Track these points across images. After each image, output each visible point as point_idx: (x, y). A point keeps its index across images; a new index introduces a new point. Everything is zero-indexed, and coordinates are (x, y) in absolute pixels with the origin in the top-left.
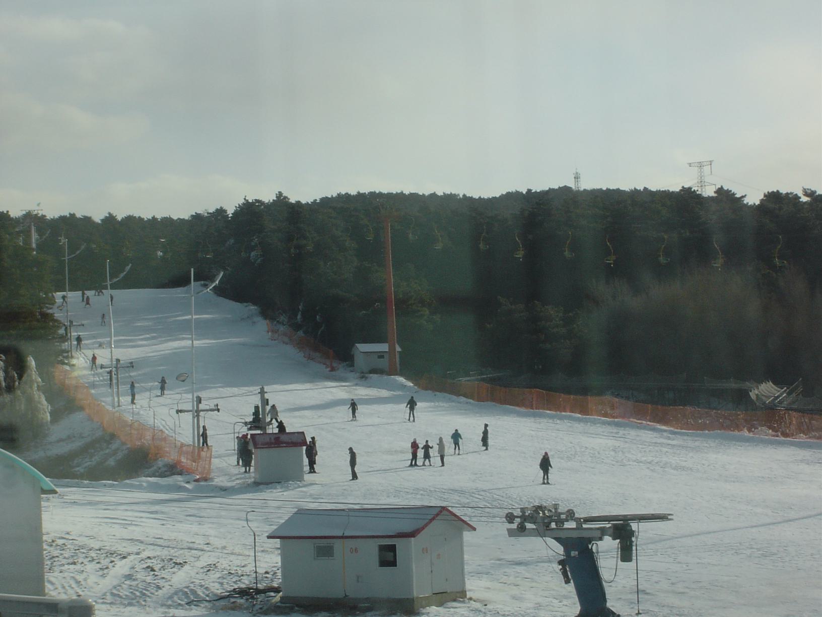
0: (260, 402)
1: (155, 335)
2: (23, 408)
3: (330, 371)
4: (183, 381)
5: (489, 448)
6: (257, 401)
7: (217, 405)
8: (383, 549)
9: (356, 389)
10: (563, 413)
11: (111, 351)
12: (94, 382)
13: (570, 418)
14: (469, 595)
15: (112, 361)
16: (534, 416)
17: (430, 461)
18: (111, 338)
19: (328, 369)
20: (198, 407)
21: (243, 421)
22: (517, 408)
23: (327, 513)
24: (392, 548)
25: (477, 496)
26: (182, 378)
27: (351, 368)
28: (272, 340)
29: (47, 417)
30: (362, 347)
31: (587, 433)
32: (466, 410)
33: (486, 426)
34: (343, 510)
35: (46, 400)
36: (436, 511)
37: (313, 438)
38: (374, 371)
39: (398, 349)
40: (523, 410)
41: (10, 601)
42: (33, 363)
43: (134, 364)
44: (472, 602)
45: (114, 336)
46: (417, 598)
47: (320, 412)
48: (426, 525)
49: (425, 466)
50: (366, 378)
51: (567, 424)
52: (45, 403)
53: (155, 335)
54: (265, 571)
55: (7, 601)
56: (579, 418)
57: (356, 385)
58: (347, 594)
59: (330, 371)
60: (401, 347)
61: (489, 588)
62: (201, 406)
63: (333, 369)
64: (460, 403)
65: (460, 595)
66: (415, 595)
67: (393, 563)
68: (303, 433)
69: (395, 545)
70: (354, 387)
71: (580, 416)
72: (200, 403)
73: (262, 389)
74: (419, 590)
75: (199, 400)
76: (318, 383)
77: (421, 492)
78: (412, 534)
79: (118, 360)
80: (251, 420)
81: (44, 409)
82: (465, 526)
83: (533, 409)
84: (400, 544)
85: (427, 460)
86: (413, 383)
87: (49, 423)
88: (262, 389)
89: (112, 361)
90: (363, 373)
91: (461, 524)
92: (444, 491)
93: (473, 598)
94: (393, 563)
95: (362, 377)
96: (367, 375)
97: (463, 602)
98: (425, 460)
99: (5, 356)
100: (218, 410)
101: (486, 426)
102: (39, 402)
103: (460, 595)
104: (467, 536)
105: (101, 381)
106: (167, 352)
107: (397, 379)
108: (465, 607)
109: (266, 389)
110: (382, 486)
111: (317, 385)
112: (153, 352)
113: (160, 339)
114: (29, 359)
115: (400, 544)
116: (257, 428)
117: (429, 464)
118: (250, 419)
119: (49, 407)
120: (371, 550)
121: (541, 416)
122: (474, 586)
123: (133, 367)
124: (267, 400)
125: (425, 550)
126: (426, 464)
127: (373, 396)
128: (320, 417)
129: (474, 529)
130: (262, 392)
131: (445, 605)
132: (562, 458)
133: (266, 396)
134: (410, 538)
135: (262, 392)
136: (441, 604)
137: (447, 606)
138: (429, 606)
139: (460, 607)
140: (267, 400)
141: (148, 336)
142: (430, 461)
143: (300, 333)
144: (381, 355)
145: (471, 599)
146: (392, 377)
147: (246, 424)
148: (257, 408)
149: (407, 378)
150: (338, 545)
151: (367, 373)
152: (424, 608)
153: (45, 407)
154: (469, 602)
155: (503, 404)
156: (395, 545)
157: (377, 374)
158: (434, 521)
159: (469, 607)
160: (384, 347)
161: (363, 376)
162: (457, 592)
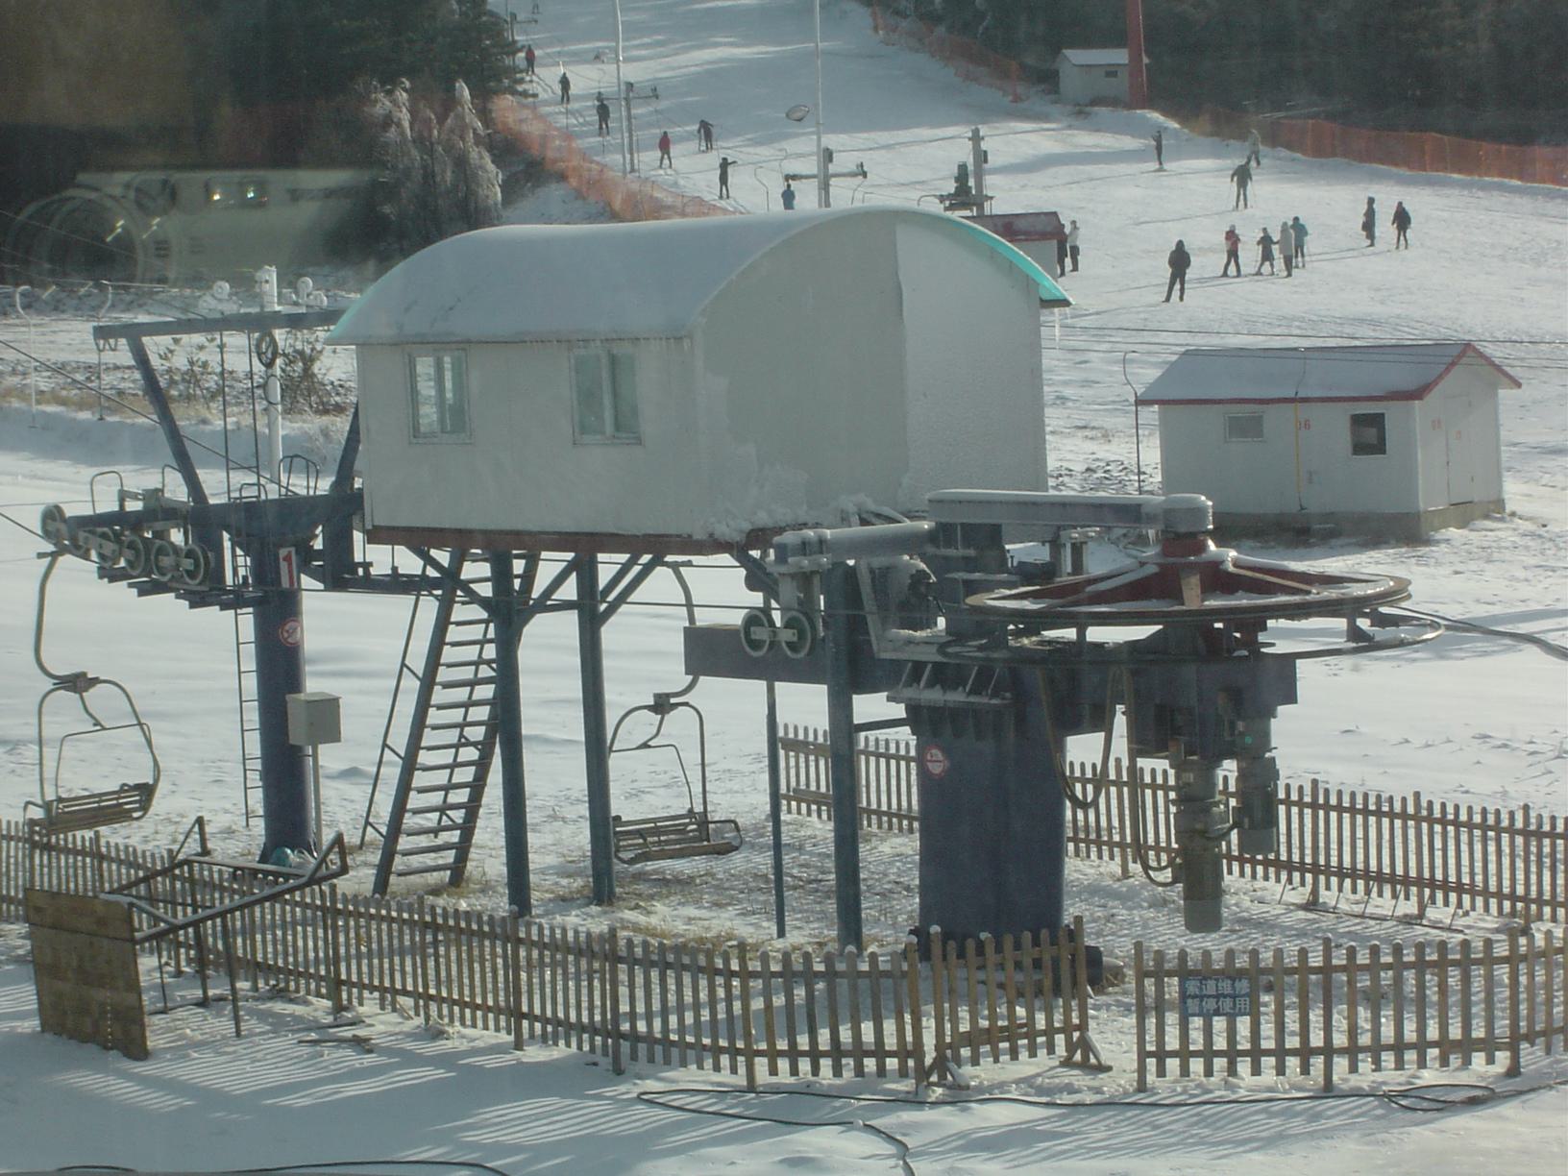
0: (971, 157)
1: (660, 37)
2: (448, 179)
3: (1012, 102)
4: (799, 120)
5: (1376, 241)
6: (964, 153)
7: (862, 165)
8: (1358, 421)
9: (1073, 135)
10: (1487, 179)
11: (618, 67)
12: (567, 127)
13: (1501, 188)
14: (1509, 508)
15: (619, 86)
16: (1430, 183)
17: (1272, 265)
18: (618, 43)
19: (1011, 98)
20: (826, 168)
21: (938, 193)
22: (1394, 170)
23: (1279, 353)
24: (1377, 421)
25: (1406, 329)
26: (799, 115)
27: (1053, 97)
28: (887, 44)
29: (496, 194)
30: (1076, 56)
31: (1545, 215)
32: (1295, 173)
33: (1371, 201)
34: (1295, 349)
35: (493, 162)
36: (1455, 352)
37: (1074, 223)
38: (1096, 102)
39: (1146, 60)
40: (1404, 172)
41: (1034, 504)
42: (466, 93)
43: (659, 92)
44: (1516, 520)
45: (623, 40)
46: (1426, 512)
47: (1022, 179)
48: (1440, 377)
49: (1261, 274)
50: (1088, 114)
51: (1498, 199)
52: (491, 167)
53: (660, 37)
54: (1086, 466)
55: (995, 502)
56: (1518, 187)
57: (1070, 127)
58: (1304, 505)
59: (1012, 102)
60: (1149, 57)
61: (1529, 495)
62: (832, 168)
63: (1017, 99)
64: (1279, 159)
65: (1494, 509)
66: (1422, 506)
67: (1379, 447)
68: (1055, 214)
69: (1383, 415)
70: (1069, 132)
71: (1519, 183)
72: (831, 160)
73: (976, 132)
74: (1429, 499)
75: (828, 156)
76: (997, 125)
77: (1297, 323)
78: (1417, 394)
79: (630, 86)
80: (952, 191)
81: (489, 179)
82: (1505, 380)
83: (1425, 170)
84: (1392, 412)
85: (1267, 263)
86: (1179, 123)
87: (500, 206)
88: (976, 132)
89: (619, 86)
90: (1079, 105)
91: (1499, 375)
92: (1338, 321)
93: (1519, 513)
94: (1379, 447)
95: (1080, 113)
96: (1088, 109)
97: (1502, 520)
98: (1262, 265)
99: (411, 83)
100: (865, 175)
101: (1371, 201)
102: (482, 167)
103: (1494, 509)
104: (1505, 394)
105: (582, 125)
106: (693, 69)
107: (1149, 116)
108: (1507, 528)
109: (983, 130)
110: (1213, 313)
111: (997, 128)
112: (664, 70)
113: (673, 46)
114: (457, 85)
115: (1392, 412)
116: (965, 205)
117: (1235, 274)
118: (951, 187)
119: (500, 176)
120: (1334, 428)
121: (1443, 184)
122: (1514, 491)
123: (657, 97)
124: (985, 152)
125: (1436, 424)
126: (1262, 271)
127: (1108, 147)
128: (1024, 186)
129: (1519, 385)
130: (976, 138)
131: (1471, 526)
132: (1523, 261)
133: (984, 146)
134: (1410, 402)
135: (976, 138)
136: (1463, 524)
137: (1474, 527)
138: (1445, 527)
139: (1499, 529)
140: (985, 152)
141: (646, 40)
142: (1272, 265)
143: (941, 30)
144: (1111, 72)
145: (1513, 514)
146: (1138, 111)
147: (942, 199)
148: (963, 168)
149: (1166, 113)
150: (1272, 416)
151: (1086, 106)
152: (1437, 530)
153: (492, 176)
154: (1512, 521)
155: (1365, 162)
156: (1383, 415)
157: (1107, 106)
158: (1457, 367)
159: (1515, 530)
160: (1119, 56)
161: (1083, 110)
162: (1489, 502)
